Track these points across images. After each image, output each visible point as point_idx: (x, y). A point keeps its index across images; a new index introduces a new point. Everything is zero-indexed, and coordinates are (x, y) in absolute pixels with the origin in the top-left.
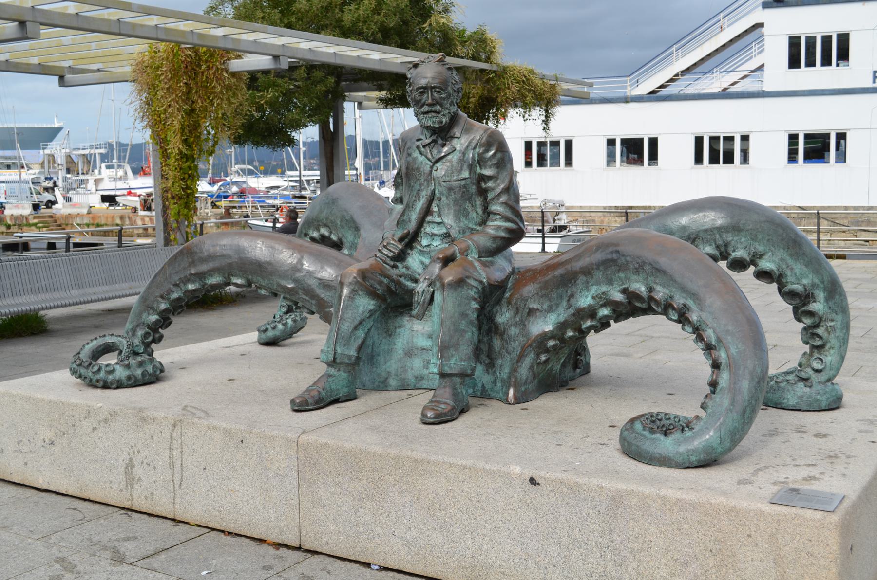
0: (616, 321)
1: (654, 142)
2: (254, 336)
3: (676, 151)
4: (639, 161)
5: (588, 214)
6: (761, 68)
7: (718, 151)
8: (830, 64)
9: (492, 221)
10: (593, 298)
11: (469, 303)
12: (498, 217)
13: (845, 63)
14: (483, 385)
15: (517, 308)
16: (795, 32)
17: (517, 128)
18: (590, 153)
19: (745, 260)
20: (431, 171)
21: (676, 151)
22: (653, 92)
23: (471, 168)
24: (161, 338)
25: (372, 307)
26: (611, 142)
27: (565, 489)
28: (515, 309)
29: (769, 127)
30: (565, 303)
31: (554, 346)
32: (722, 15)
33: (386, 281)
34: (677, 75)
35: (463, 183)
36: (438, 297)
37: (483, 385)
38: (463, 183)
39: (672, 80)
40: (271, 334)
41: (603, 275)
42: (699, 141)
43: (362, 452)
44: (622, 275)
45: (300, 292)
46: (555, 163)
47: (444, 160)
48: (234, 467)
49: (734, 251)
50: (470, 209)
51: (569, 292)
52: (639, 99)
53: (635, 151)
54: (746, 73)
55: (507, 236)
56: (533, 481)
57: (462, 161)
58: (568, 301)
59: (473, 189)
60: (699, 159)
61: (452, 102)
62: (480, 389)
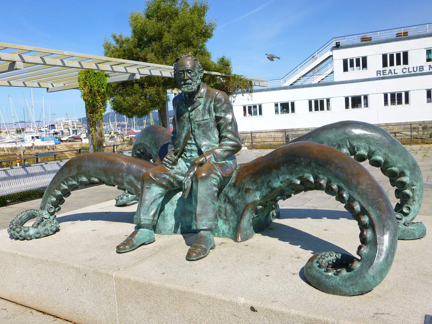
0: (294, 194)
1: (293, 104)
2: (114, 202)
3: (302, 107)
4: (288, 112)
5: (269, 133)
6: (332, 72)
7: (319, 105)
8: (400, 64)
9: (223, 141)
10: (281, 182)
11: (212, 188)
12: (227, 139)
13: (366, 69)
14: (223, 231)
15: (239, 189)
16: (384, 52)
17: (239, 101)
18: (269, 109)
19: (365, 155)
20: (189, 116)
21: (302, 107)
22: (291, 85)
23: (209, 112)
24: (60, 209)
25: (160, 192)
26: (276, 105)
27: (274, 316)
28: (238, 189)
29: (337, 95)
30: (266, 185)
31: (261, 209)
32: (316, 53)
33: (168, 177)
34: (300, 77)
35: (206, 121)
36: (263, 118)
37: (223, 231)
38: (206, 121)
39: (298, 79)
40: (121, 201)
41: (287, 169)
42: (310, 102)
43: (150, 285)
44: (297, 169)
45: (125, 183)
46: (255, 114)
47: (195, 110)
48: (82, 289)
49: (358, 150)
50: (211, 136)
51: (268, 180)
52: (285, 88)
53: (286, 107)
54: (327, 75)
55: (232, 149)
56: (253, 309)
57: (204, 109)
58: (268, 184)
59: (212, 124)
60: (311, 109)
61: (198, 78)
62: (221, 232)
